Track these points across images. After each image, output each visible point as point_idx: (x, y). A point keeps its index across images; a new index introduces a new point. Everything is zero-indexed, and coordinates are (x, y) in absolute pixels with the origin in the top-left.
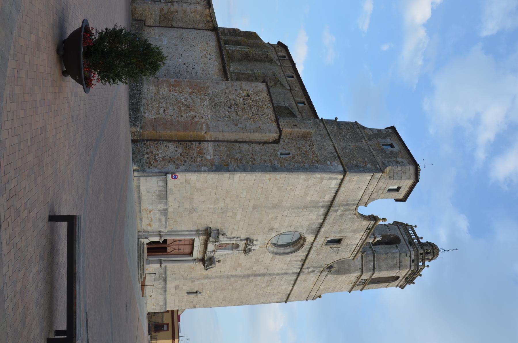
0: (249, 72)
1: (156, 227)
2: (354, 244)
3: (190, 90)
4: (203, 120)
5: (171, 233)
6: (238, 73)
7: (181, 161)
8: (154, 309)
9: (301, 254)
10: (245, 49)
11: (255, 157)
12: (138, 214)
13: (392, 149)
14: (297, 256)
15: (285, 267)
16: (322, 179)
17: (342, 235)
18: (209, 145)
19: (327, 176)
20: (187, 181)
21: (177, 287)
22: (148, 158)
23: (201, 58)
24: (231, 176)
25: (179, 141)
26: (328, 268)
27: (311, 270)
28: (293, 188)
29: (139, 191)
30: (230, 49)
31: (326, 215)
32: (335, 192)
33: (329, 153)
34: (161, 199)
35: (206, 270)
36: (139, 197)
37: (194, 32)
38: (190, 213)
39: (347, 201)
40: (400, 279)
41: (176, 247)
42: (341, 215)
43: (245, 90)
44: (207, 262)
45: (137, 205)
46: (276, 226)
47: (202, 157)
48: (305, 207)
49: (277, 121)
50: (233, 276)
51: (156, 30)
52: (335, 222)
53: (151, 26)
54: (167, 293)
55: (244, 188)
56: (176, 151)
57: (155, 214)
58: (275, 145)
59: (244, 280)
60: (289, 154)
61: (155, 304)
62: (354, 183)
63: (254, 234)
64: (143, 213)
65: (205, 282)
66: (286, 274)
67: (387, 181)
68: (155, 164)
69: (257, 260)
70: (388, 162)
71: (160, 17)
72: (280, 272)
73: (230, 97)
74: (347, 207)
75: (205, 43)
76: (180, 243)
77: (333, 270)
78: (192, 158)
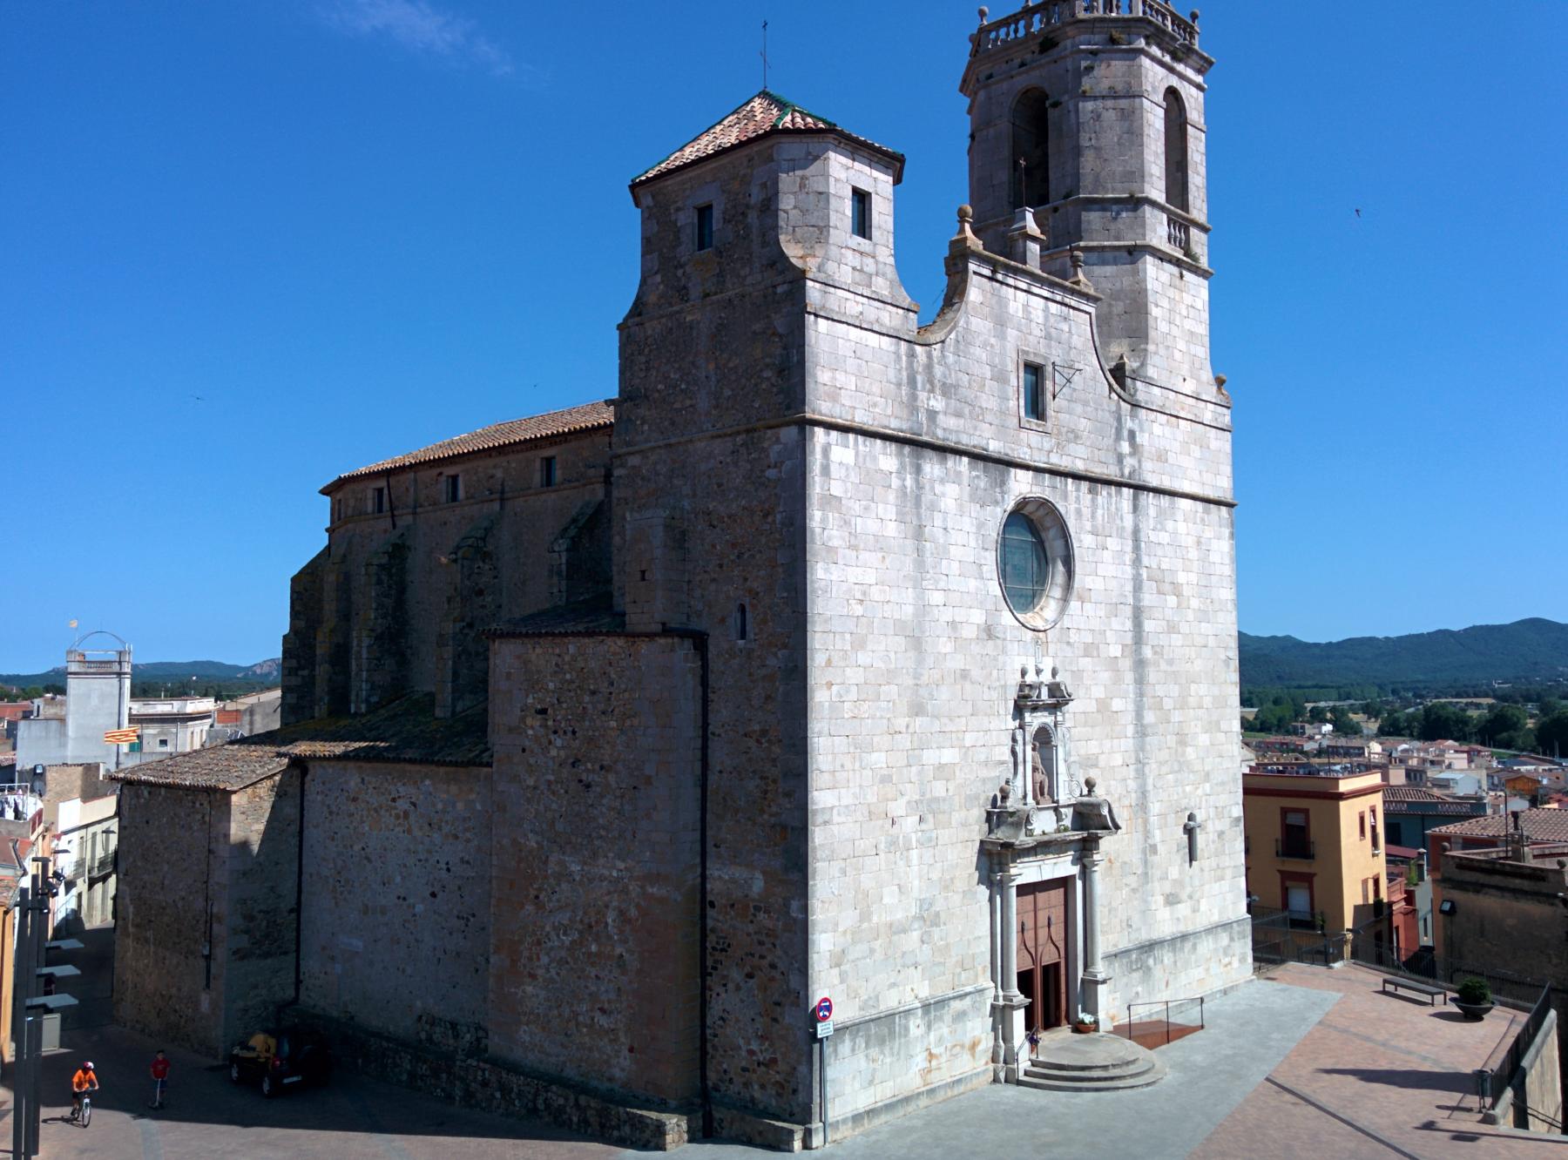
0: (448, 652)
1: (980, 1027)
2: (1046, 309)
3: (530, 908)
4: (634, 888)
5: (998, 970)
6: (453, 692)
7: (772, 979)
8: (1242, 960)
9: (1073, 503)
10: (362, 645)
11: (757, 727)
12: (941, 1096)
13: (717, 214)
14: (1079, 512)
15: (1113, 543)
16: (830, 500)
17: (1011, 367)
18: (716, 874)
19: (816, 487)
20: (837, 961)
21: (1171, 900)
22: (763, 1087)
23: (409, 831)
24: (819, 819)
25: (704, 974)
26: (1122, 386)
27: (1125, 447)
28: (859, 596)
29: (871, 1113)
30: (367, 701)
31: (943, 450)
32: (869, 441)
33: (736, 464)
34: (892, 1033)
35: (1117, 827)
36: (889, 1107)
37: (311, 834)
38: (935, 921)
39: (899, 385)
40: (1174, 81)
41: (1043, 933)
42: (944, 394)
43: (523, 719)
44: (1090, 823)
45: (911, 1108)
46: (978, 617)
47: (757, 908)
48: (919, 534)
49: (635, 635)
50: (1139, 715)
51: (311, 965)
52: (967, 411)
53: (298, 982)
54: (1190, 929)
55: (857, 765)
56: (738, 988)
57: (940, 1040)
58: (712, 651)
59: (1152, 675)
60: (742, 609)
61: (1227, 960)
62: (841, 378)
63: (1004, 687)
64: (938, 1078)
65: (1155, 808)
66: (1136, 532)
67: (833, 251)
68: (782, 1066)
69: (1089, 650)
70: (764, 244)
71: (267, 955)
72: (1128, 558)
73: (552, 778)
74: (919, 378)
75: (352, 808)
76: (1029, 924)
77: (1131, 364)
78: (761, 943)
